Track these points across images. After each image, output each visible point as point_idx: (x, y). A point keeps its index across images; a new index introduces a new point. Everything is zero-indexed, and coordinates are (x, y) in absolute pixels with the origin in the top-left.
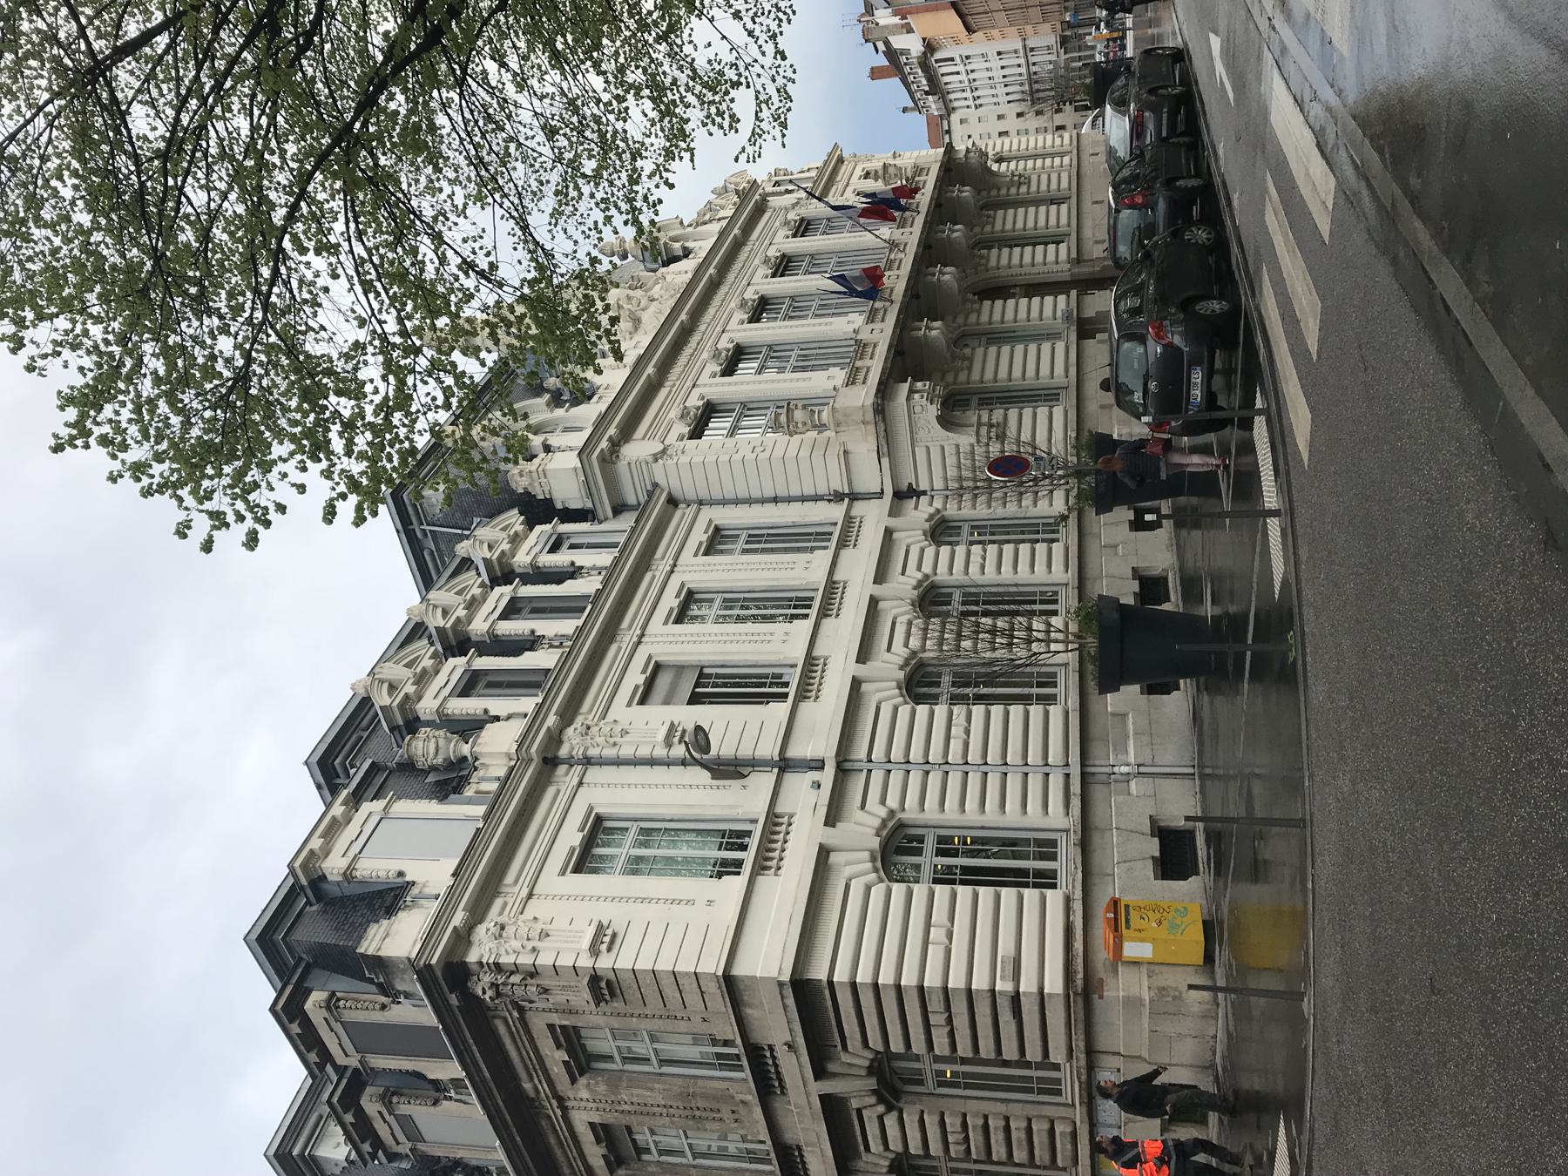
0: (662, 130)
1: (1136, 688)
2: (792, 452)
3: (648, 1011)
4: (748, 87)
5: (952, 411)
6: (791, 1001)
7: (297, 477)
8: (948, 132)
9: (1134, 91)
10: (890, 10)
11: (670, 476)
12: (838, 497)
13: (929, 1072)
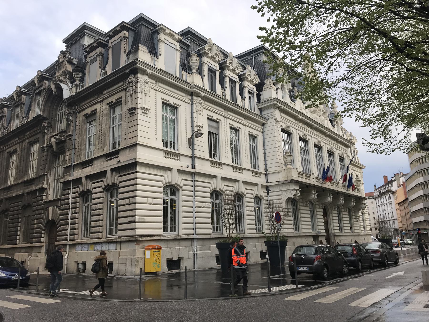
0: (371, 117)
1: (217, 252)
2: (278, 157)
3: (127, 124)
4: (384, 141)
5: (292, 201)
6: (131, 162)
7: (272, 19)
8: (369, 198)
9: (386, 250)
10: (404, 181)
11: (270, 123)
12: (266, 170)
13: (88, 204)
